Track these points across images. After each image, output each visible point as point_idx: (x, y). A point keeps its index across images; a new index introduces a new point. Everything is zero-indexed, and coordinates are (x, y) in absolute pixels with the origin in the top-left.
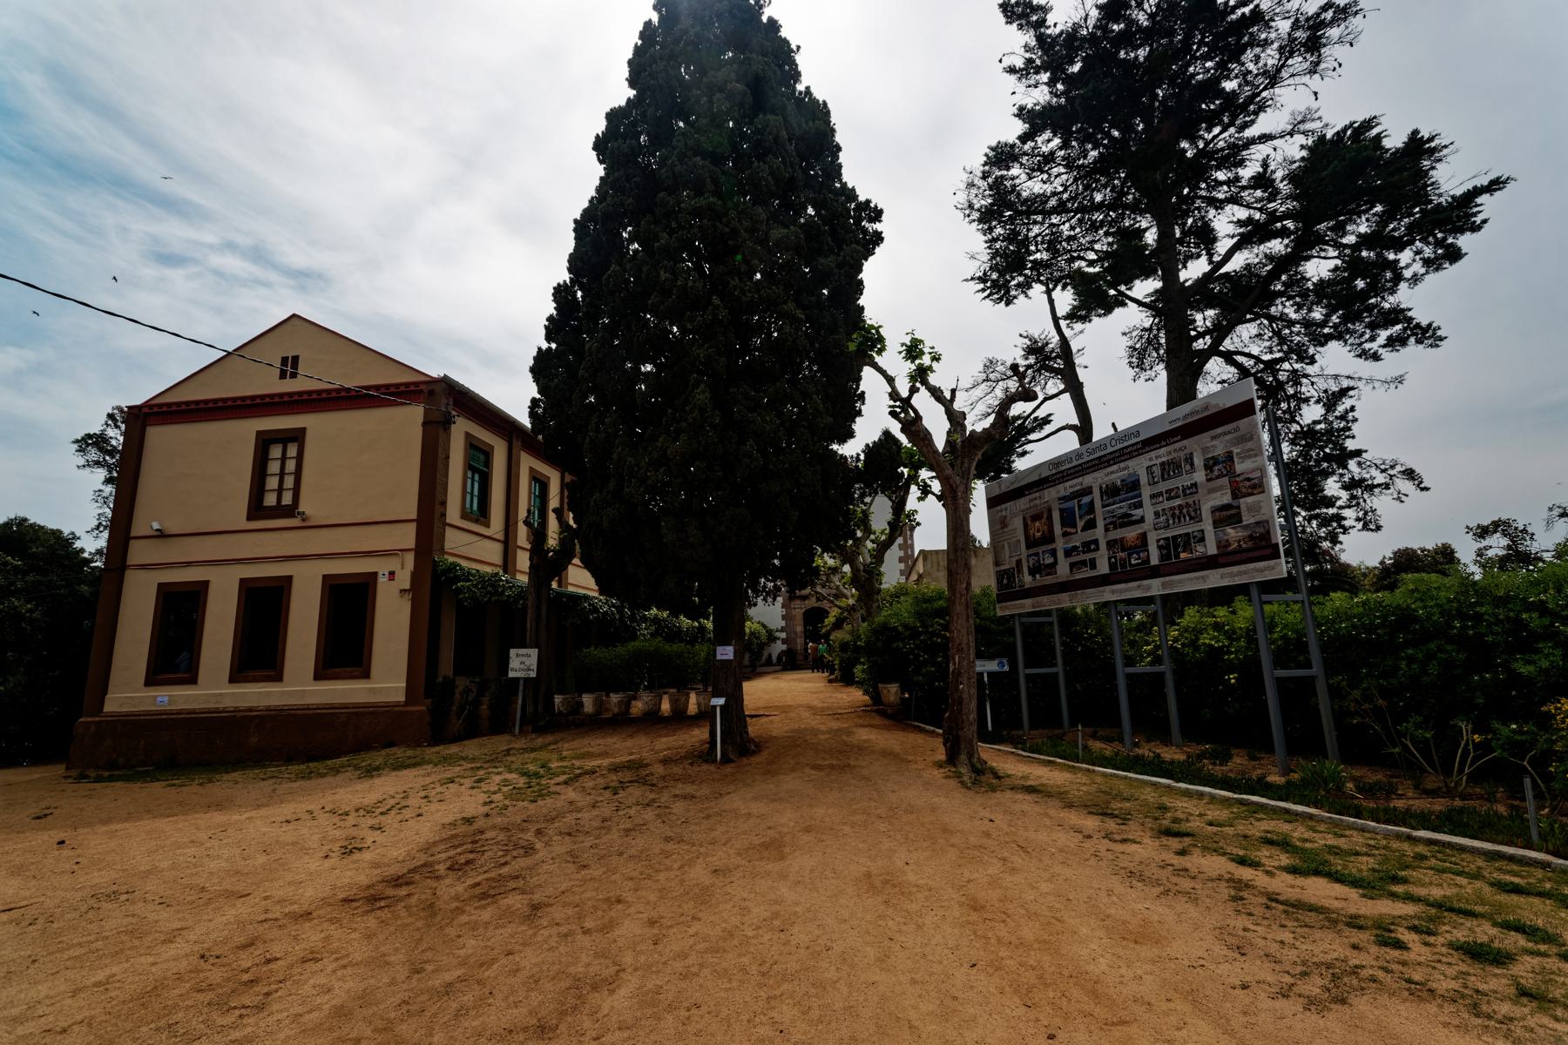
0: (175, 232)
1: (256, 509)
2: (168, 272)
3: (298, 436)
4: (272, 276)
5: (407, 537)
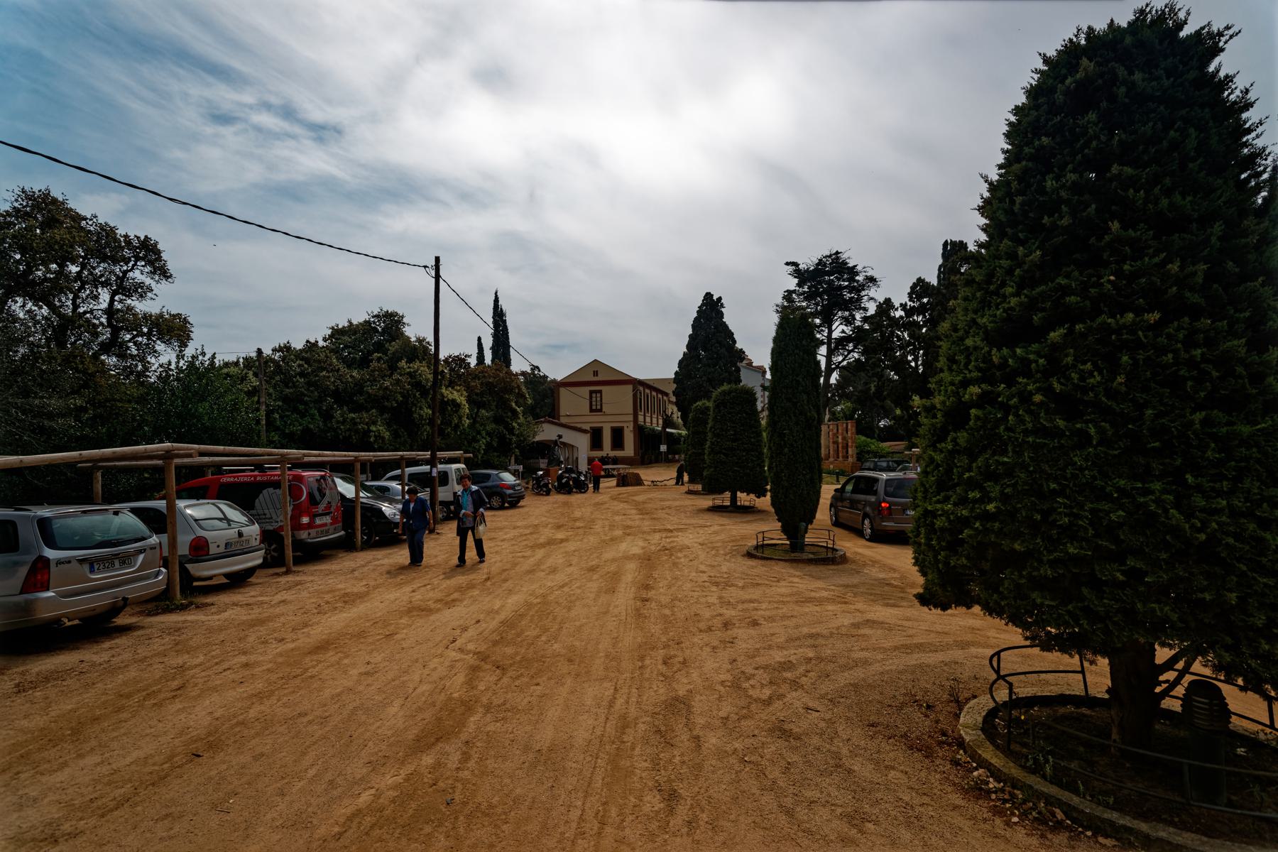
0: (226, 96)
1: (592, 410)
2: (223, 130)
3: (600, 392)
4: (297, 130)
5: (631, 418)
